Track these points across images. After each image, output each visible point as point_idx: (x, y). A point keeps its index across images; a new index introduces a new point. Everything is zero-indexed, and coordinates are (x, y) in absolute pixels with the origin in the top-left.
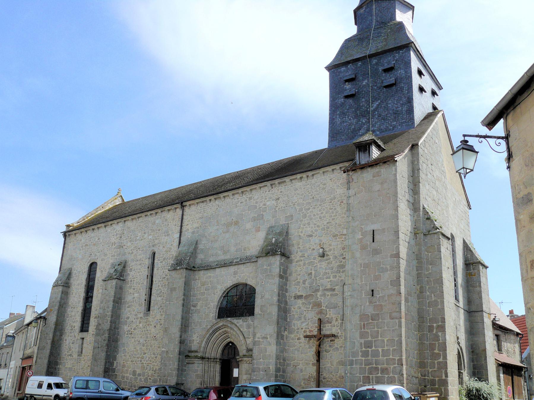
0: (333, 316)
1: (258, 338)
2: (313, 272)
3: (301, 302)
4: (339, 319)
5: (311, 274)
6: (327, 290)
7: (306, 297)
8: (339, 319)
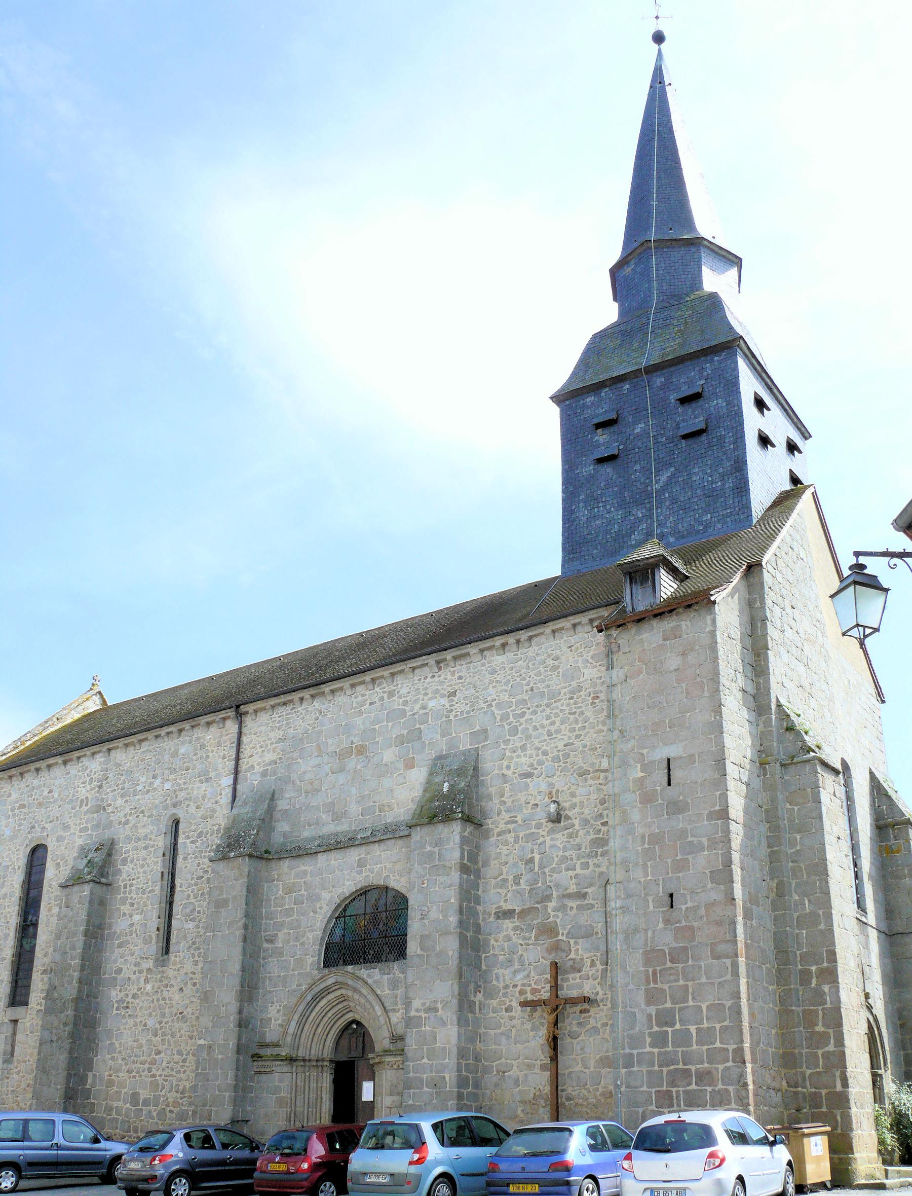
0: (585, 956)
1: (417, 1010)
2: (537, 857)
3: (511, 925)
4: (598, 963)
5: (531, 860)
6: (569, 896)
7: (523, 914)
8: (598, 963)
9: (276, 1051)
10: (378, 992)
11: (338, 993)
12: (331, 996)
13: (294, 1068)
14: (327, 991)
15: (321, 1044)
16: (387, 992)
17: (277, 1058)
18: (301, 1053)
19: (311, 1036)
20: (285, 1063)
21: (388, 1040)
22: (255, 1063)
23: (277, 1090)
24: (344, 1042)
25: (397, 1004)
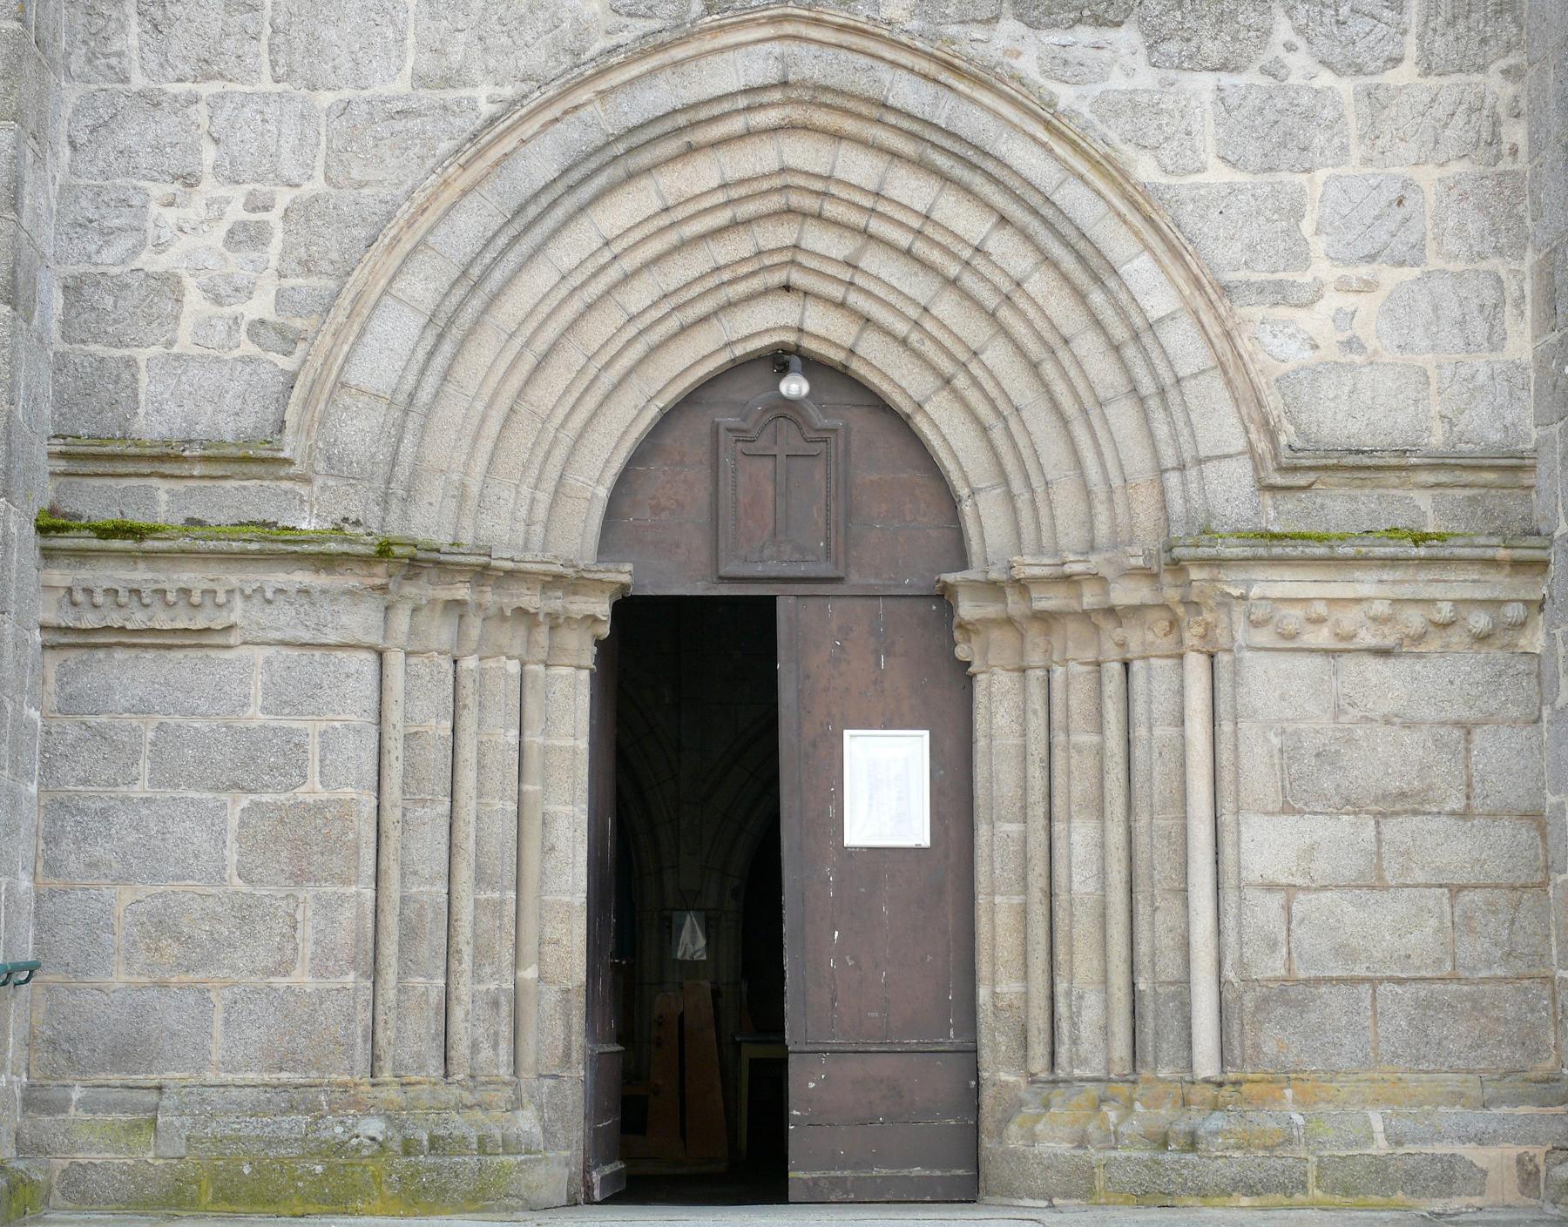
9: (234, 500)
10: (1145, 170)
11: (759, 158)
12: (703, 174)
13: (402, 620)
14: (682, 132)
15: (538, 464)
16: (1218, 175)
17: (275, 547)
18: (429, 522)
19: (493, 427)
20: (350, 580)
21: (1241, 471)
22: (60, 576)
23: (262, 760)
24: (682, 484)
25: (1300, 257)
